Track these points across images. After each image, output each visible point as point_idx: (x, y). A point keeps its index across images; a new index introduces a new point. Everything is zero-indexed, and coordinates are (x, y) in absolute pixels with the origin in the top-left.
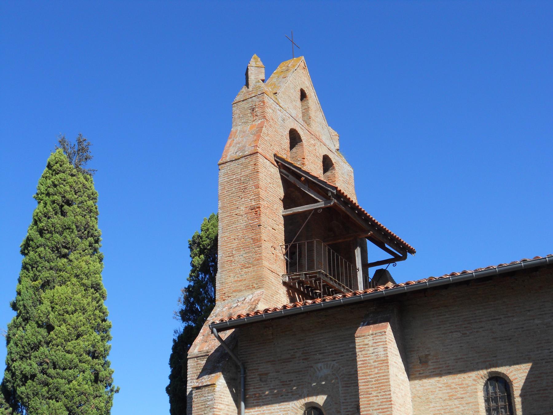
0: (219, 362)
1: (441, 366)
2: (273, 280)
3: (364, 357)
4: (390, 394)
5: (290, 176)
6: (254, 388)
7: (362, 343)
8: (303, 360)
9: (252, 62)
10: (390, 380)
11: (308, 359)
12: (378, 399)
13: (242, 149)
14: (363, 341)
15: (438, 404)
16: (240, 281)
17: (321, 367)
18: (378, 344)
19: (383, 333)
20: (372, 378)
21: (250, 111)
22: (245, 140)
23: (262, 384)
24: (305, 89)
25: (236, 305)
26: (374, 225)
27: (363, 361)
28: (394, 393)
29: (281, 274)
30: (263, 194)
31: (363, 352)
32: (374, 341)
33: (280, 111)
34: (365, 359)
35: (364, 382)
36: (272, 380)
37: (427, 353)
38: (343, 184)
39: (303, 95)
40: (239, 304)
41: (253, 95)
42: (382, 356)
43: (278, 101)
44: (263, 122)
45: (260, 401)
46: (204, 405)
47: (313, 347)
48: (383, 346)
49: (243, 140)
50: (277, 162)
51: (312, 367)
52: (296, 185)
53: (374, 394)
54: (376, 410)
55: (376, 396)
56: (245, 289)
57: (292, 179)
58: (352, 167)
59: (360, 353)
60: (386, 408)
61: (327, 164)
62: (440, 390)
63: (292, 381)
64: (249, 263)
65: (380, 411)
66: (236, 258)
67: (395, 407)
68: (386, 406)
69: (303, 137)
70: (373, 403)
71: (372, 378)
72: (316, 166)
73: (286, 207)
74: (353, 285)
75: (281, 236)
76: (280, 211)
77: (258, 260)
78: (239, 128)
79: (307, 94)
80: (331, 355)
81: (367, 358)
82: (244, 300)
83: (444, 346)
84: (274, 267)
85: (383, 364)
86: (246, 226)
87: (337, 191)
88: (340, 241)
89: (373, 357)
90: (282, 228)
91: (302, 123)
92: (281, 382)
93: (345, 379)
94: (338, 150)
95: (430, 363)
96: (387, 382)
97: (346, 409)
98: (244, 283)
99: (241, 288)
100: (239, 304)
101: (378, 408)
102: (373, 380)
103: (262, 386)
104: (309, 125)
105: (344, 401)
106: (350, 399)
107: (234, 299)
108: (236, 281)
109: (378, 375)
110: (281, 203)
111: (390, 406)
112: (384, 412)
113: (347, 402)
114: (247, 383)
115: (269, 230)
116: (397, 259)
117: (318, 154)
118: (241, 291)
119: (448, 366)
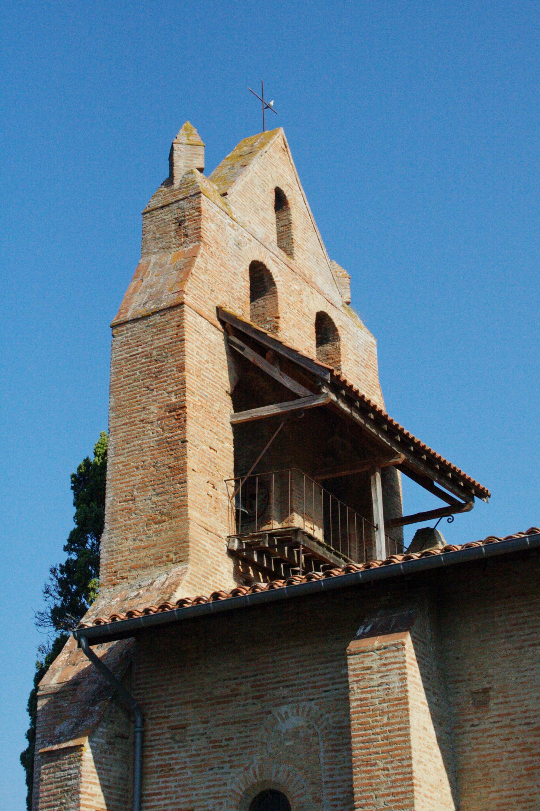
0: (94, 703)
1: (512, 711)
2: (208, 547)
3: (362, 693)
4: (410, 766)
5: (248, 349)
6: (160, 755)
7: (361, 666)
8: (253, 698)
9: (182, 137)
10: (412, 737)
11: (263, 696)
12: (387, 776)
13: (155, 297)
14: (362, 662)
15: (505, 786)
16: (144, 548)
17: (286, 713)
18: (389, 667)
19: (400, 647)
20: (377, 734)
21: (173, 227)
22: (162, 281)
23: (176, 746)
24: (285, 189)
25: (135, 593)
26: (407, 443)
27: (361, 700)
28: (420, 762)
29: (225, 535)
30: (191, 381)
31: (361, 683)
32: (383, 661)
33: (232, 227)
34: (364, 696)
35: (363, 742)
36: (194, 738)
37: (487, 686)
38: (356, 368)
39: (281, 201)
40: (141, 592)
41: (181, 197)
42: (397, 690)
43: (230, 210)
44: (198, 247)
45: (172, 778)
46: (62, 787)
47: (271, 675)
48: (398, 671)
49: (158, 282)
50: (223, 323)
51: (270, 712)
52: (257, 363)
53: (381, 765)
54: (383, 796)
55: (384, 769)
56: (155, 564)
57: (250, 354)
58: (376, 335)
59: (355, 686)
60: (402, 793)
61: (325, 329)
62: (510, 758)
63: (232, 739)
64: (162, 514)
65: (391, 798)
66: (140, 505)
67: (421, 790)
68: (403, 789)
69: (277, 278)
70: (378, 784)
71: (377, 734)
72: (302, 333)
73: (238, 407)
74: (367, 553)
75: (228, 464)
76: (225, 412)
77: (179, 507)
78: (153, 259)
79: (288, 198)
80: (306, 688)
81: (369, 696)
82: (152, 584)
83: (519, 672)
84: (212, 521)
85: (399, 707)
86: (160, 443)
87: (332, 375)
88: (344, 473)
89: (381, 693)
90: (229, 447)
91: (278, 251)
92: (211, 742)
93: (332, 736)
94: (348, 303)
95: (491, 703)
96: (405, 741)
97: (332, 794)
98: (153, 551)
99: (146, 560)
100: (141, 592)
101: (387, 792)
102: (379, 737)
103: (176, 749)
104: (290, 254)
105: (327, 779)
106: (340, 775)
107: (132, 582)
108: (138, 549)
109: (389, 728)
110: (229, 399)
111: (410, 788)
112: (397, 801)
113: (335, 782)
114: (148, 744)
115: (203, 450)
116: (455, 508)
117: (306, 311)
118: (145, 567)
119: (525, 712)
